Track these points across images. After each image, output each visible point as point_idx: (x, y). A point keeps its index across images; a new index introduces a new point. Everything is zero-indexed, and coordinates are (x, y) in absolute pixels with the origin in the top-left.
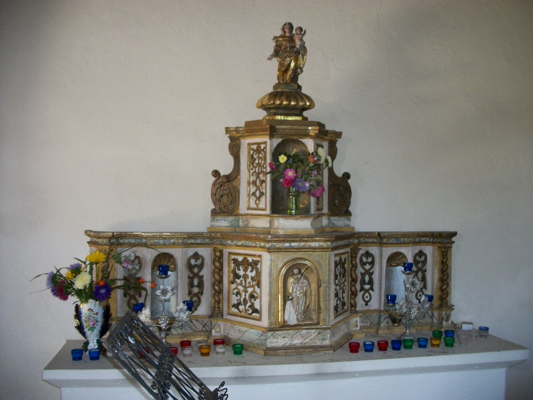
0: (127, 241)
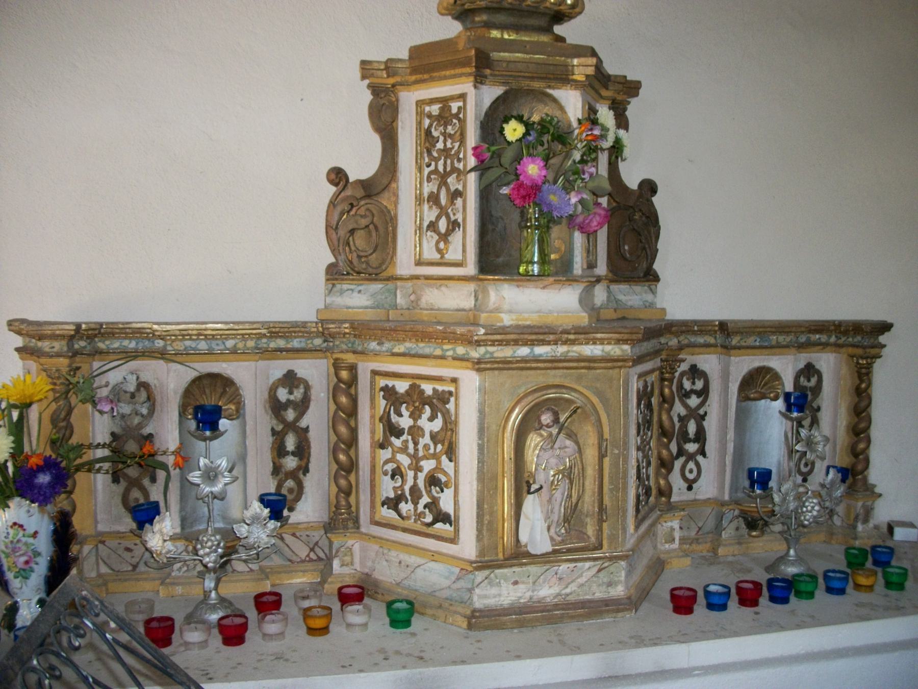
0: (116, 344)
